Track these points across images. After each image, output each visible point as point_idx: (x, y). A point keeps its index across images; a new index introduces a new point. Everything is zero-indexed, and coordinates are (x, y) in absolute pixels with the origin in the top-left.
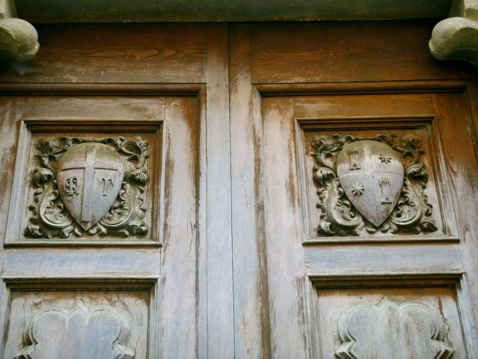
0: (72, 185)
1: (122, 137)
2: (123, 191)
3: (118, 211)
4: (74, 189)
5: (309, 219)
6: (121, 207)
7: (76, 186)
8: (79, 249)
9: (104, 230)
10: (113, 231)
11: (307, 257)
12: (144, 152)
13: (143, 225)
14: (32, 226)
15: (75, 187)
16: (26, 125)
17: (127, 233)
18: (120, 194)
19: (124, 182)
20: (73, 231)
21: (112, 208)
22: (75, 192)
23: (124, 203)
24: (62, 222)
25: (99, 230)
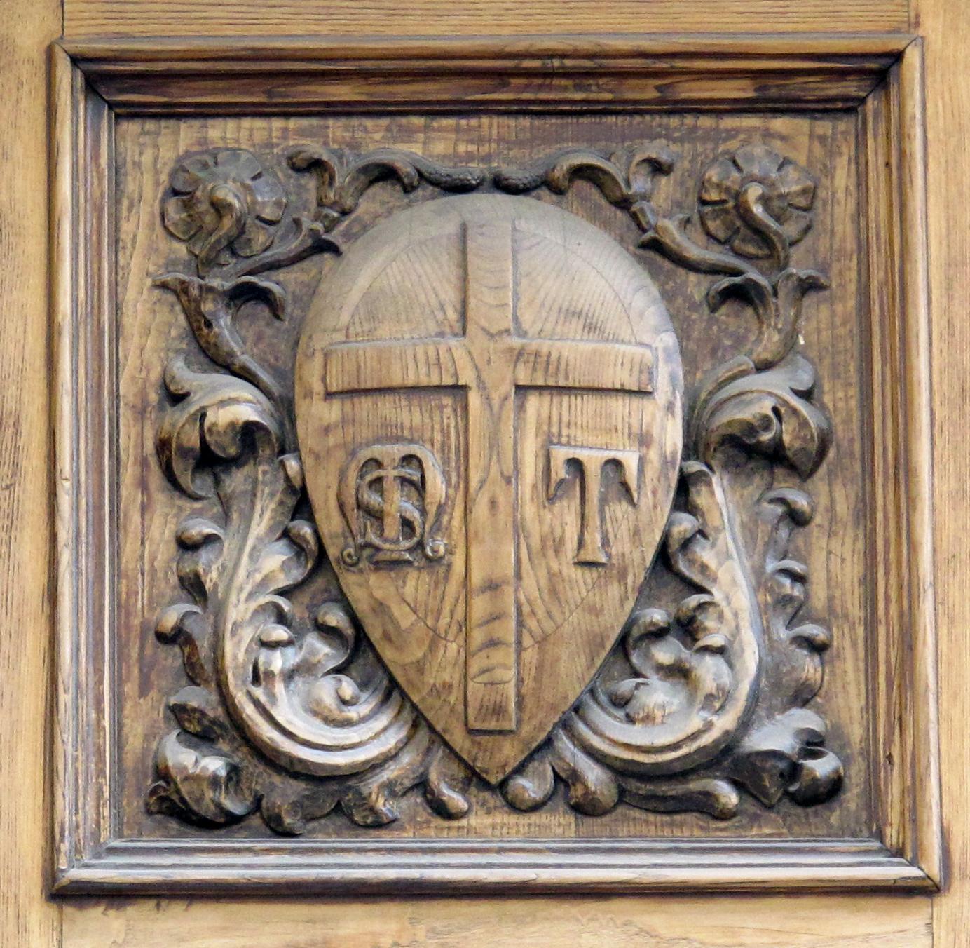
0: (399, 503)
1: (657, 150)
2: (685, 524)
3: (665, 653)
4: (407, 524)
5: (901, 735)
6: (687, 628)
7: (423, 512)
8: (58, 638)
9: (594, 777)
10: (658, 790)
11: (866, 833)
12: (792, 250)
13: (270, 776)
14: (182, 757)
15: (415, 515)
16: (80, 82)
17: (728, 796)
18: (674, 546)
19: (695, 466)
20: (422, 785)
21: (626, 644)
22: (420, 545)
23: (701, 606)
24: (365, 736)
25: (565, 780)
